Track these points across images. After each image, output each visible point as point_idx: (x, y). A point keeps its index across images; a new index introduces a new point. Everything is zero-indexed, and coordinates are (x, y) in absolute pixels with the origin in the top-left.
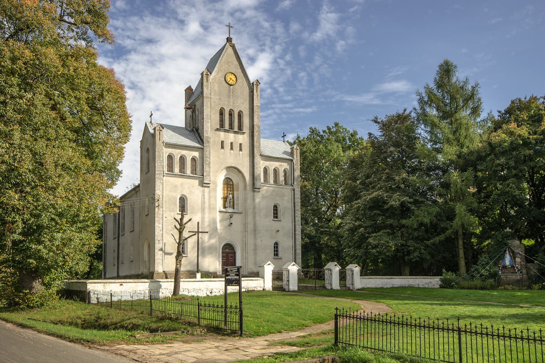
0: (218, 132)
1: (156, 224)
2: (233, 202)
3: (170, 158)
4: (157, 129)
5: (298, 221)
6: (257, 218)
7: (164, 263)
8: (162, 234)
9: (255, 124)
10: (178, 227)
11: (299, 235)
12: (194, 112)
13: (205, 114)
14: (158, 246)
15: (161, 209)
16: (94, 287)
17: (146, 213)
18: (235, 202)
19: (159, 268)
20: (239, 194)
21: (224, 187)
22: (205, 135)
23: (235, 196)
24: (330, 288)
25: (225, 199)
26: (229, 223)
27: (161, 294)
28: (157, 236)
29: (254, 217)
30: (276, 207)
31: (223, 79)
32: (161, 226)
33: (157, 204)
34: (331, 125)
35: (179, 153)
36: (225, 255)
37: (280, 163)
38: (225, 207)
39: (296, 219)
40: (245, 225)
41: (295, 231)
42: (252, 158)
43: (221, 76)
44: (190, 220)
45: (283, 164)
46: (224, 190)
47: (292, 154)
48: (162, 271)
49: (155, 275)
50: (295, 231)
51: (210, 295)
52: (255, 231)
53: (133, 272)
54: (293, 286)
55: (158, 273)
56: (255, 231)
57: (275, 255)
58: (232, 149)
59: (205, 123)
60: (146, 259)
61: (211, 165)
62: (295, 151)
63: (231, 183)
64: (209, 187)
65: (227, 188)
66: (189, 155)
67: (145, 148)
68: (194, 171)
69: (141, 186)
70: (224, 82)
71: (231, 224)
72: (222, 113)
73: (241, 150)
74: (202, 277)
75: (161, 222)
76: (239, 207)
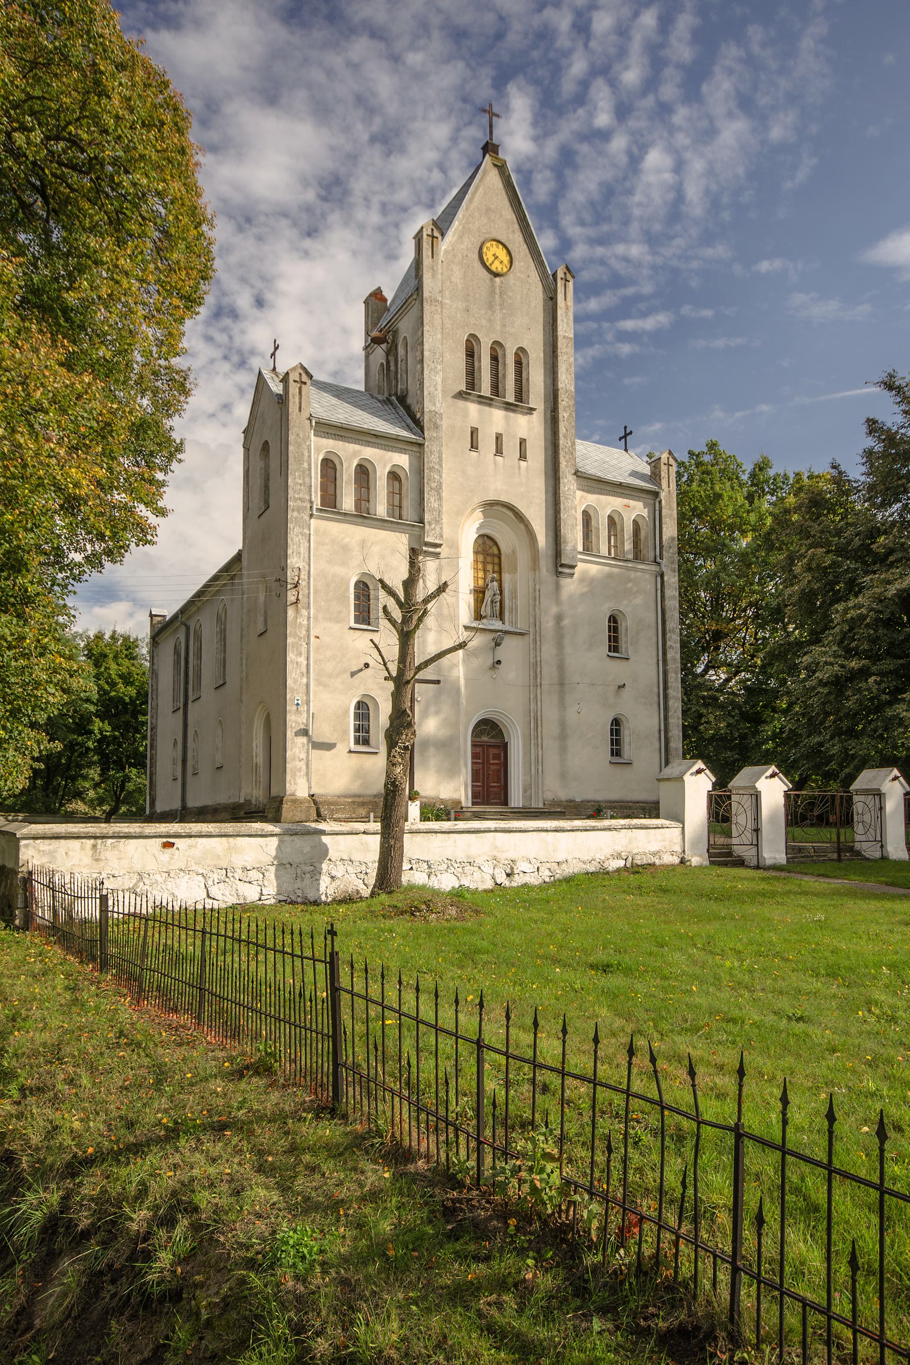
0: (461, 403)
1: (291, 656)
2: (501, 602)
3: (329, 466)
4: (292, 377)
5: (674, 659)
6: (568, 650)
7: (324, 766)
8: (308, 685)
9: (560, 385)
10: (397, 615)
11: (676, 698)
12: (392, 351)
13: (426, 347)
14: (294, 721)
15: (304, 612)
16: (52, 854)
17: (261, 629)
18: (507, 603)
19: (298, 787)
20: (517, 580)
21: (476, 561)
22: (428, 406)
23: (506, 586)
24: (878, 855)
25: (479, 593)
26: (490, 662)
27: (324, 881)
28: (293, 690)
29: (560, 646)
30: (615, 621)
31: (476, 257)
32: (302, 660)
33: (291, 598)
34: (700, 447)
35: (355, 454)
36: (479, 750)
37: (626, 501)
38: (478, 617)
39: (669, 656)
40: (535, 668)
41: (666, 688)
42: (551, 482)
43: (469, 245)
44: (442, 588)
45: (632, 503)
46: (476, 569)
47: (655, 476)
48: (306, 795)
49: (285, 806)
50: (666, 688)
51: (506, 882)
52: (562, 684)
53: (223, 798)
54: (774, 851)
55: (295, 801)
56: (562, 684)
57: (612, 755)
58: (499, 451)
59: (426, 372)
60: (260, 759)
61: (444, 494)
62: (664, 468)
63: (496, 551)
64: (437, 555)
65: (484, 563)
66: (385, 461)
67: (257, 445)
68: (396, 508)
69: (245, 556)
70: (477, 265)
71: (499, 662)
72: (471, 353)
73: (523, 457)
74: (424, 818)
75: (304, 649)
76: (518, 619)
